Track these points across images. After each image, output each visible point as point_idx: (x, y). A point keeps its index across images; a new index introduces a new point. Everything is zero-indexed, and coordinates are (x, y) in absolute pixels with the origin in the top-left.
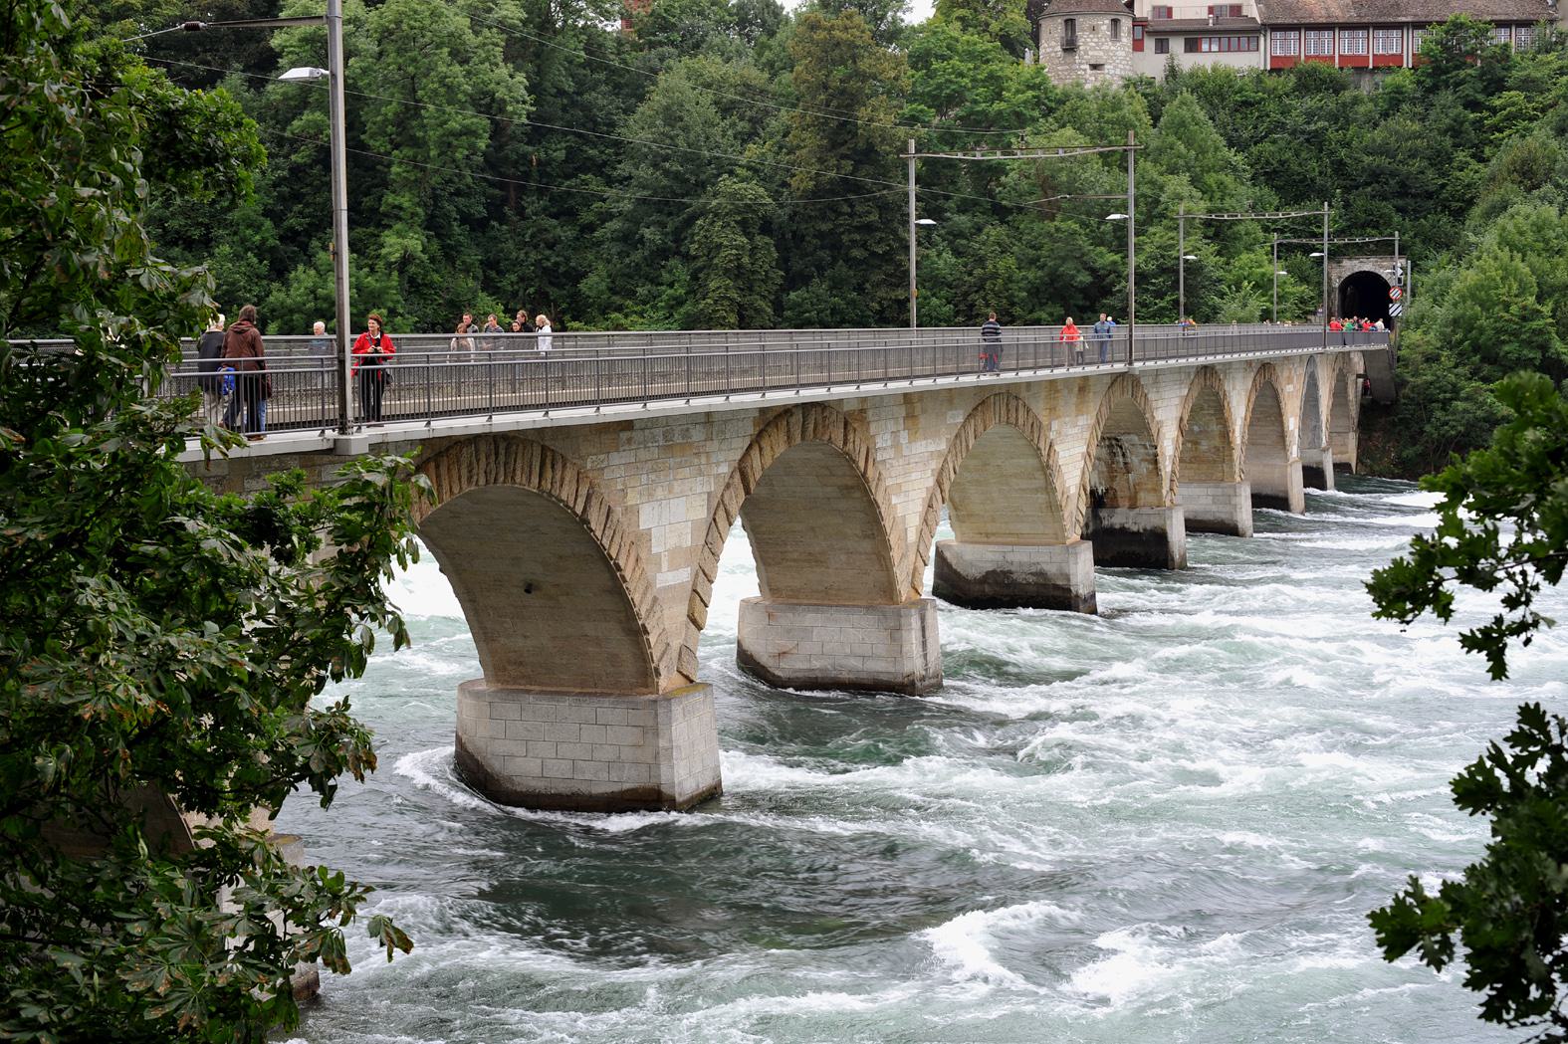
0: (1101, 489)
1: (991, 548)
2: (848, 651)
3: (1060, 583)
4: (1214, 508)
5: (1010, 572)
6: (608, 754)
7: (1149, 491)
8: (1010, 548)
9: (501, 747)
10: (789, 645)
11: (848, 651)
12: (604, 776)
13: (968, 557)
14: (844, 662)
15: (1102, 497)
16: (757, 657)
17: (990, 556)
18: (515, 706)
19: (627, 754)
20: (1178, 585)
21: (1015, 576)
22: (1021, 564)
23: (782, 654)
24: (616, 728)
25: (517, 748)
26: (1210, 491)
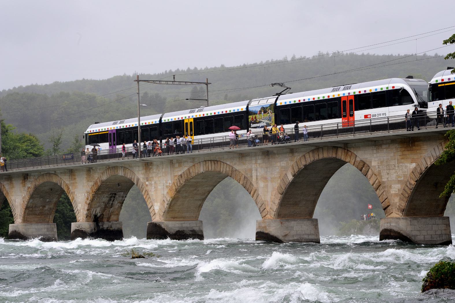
0: (99, 215)
1: (177, 222)
2: (304, 233)
3: (200, 233)
4: (48, 233)
5: (184, 231)
6: (439, 232)
7: (115, 215)
8: (183, 222)
9: (414, 233)
10: (287, 232)
11: (304, 233)
12: (439, 239)
13: (170, 226)
14: (303, 237)
15: (98, 218)
16: (278, 237)
17: (177, 225)
18: (416, 221)
19: (444, 232)
20: (168, 244)
21: (186, 232)
22: (187, 228)
23: (286, 235)
24: (440, 225)
25: (417, 233)
26: (46, 226)
